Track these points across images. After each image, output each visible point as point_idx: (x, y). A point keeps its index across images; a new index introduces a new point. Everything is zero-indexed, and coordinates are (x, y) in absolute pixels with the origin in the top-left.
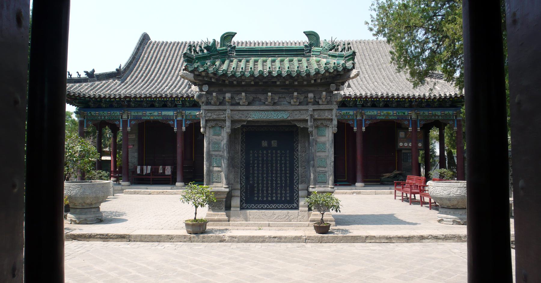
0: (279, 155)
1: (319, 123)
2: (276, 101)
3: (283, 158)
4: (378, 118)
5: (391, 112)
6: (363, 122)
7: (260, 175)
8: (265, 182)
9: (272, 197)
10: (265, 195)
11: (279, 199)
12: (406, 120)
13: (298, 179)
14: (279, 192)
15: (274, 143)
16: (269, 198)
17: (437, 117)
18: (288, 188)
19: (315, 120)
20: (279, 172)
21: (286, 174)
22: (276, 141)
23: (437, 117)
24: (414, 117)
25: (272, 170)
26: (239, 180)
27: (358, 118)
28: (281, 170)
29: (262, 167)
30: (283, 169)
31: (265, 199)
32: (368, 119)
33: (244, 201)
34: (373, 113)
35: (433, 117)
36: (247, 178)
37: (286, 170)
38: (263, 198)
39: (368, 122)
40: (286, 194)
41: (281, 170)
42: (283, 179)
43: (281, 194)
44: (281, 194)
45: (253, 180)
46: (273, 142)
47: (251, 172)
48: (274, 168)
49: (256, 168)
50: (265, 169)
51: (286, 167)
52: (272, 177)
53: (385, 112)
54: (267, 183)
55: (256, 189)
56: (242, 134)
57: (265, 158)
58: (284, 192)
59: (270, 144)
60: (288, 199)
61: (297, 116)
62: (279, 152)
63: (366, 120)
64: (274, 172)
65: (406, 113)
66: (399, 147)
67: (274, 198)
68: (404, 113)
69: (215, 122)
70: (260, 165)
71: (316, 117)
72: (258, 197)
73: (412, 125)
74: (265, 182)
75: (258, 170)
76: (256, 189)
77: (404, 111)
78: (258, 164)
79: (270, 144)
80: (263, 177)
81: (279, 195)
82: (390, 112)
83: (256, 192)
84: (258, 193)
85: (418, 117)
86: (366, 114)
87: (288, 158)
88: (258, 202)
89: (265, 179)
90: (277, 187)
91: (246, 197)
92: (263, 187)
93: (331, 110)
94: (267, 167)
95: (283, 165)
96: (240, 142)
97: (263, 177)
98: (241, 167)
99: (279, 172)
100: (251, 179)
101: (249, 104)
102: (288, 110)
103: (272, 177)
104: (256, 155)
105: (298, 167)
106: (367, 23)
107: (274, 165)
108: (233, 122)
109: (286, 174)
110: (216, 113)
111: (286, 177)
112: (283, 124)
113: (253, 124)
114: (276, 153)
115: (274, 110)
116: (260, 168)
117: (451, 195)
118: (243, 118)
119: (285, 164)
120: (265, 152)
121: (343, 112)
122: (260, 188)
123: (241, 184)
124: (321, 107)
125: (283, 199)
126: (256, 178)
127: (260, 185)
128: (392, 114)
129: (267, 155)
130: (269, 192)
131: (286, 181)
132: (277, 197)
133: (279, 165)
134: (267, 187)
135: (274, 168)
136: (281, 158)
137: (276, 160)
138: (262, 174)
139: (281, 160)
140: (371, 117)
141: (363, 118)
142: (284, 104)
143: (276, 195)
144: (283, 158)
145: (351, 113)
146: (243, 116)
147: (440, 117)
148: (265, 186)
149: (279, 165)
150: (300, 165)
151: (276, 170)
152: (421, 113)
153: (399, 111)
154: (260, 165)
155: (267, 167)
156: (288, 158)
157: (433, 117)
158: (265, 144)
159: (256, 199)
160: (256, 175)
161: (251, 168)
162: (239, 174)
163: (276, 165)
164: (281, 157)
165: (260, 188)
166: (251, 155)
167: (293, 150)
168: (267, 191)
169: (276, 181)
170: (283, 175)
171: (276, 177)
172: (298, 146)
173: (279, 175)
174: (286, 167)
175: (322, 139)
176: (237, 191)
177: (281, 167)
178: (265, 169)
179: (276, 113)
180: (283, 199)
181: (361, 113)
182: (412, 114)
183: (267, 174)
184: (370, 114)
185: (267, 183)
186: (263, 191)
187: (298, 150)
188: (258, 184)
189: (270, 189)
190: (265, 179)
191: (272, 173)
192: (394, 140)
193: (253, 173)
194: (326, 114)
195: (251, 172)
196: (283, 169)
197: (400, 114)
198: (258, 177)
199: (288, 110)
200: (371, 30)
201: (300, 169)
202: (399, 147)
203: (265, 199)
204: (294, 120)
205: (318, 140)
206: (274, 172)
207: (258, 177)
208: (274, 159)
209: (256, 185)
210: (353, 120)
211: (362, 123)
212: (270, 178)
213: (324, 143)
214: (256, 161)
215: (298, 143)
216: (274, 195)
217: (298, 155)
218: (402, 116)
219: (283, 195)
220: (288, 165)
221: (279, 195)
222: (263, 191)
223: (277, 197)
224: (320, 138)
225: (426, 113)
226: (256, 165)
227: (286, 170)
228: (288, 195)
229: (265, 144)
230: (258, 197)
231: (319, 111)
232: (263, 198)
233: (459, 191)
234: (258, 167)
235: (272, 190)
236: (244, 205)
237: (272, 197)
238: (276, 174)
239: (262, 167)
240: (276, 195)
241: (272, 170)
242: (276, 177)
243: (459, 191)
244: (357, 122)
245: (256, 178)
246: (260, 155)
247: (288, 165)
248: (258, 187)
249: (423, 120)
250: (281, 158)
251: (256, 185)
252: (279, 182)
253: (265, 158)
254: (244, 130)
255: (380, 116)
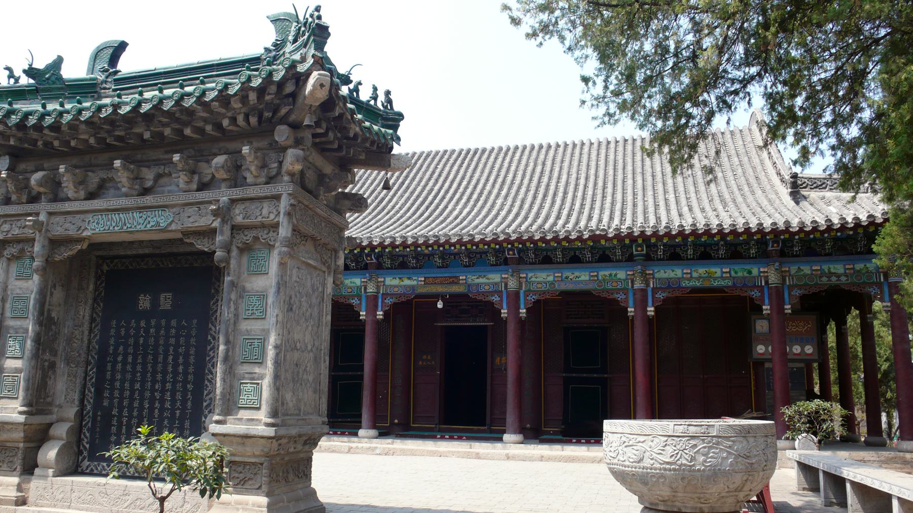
1: (248, 237)
2: (149, 184)
3: (182, 340)
4: (685, 284)
5: (717, 271)
6: (650, 294)
8: (136, 404)
12: (755, 286)
15: (166, 301)
17: (834, 279)
19: (236, 229)
20: (169, 377)
23: (834, 279)
24: (773, 278)
25: (154, 373)
27: (638, 285)
28: (175, 373)
30: (181, 369)
32: (660, 288)
33: (85, 454)
34: (672, 275)
35: (825, 279)
37: (186, 373)
39: (660, 296)
41: (175, 373)
42: (179, 396)
45: (111, 398)
48: (160, 367)
51: (186, 364)
53: (702, 271)
56: (98, 278)
57: (141, 341)
59: (155, 303)
61: (191, 220)
62: (174, 323)
63: (655, 290)
65: (755, 272)
66: (755, 356)
68: (750, 272)
69: (20, 246)
70: (130, 359)
71: (239, 219)
73: (769, 298)
74: (136, 404)
77: (748, 267)
78: (125, 355)
79: (155, 303)
82: (713, 270)
83: (114, 429)
85: (784, 280)
86: (657, 275)
87: (193, 341)
93: (277, 198)
95: (181, 360)
99: (169, 377)
100: (106, 394)
101: (91, 196)
102: (173, 206)
103: (153, 390)
104: (123, 333)
106: (506, 8)
107: (161, 358)
108: (55, 243)
109: (185, 382)
110: (19, 224)
111: (185, 391)
113: (122, 253)
114: (168, 327)
115: (141, 209)
117: (647, 463)
118: (72, 232)
119: (186, 355)
121: (601, 273)
124: (252, 192)
126: (116, 394)
128: (718, 274)
129: (147, 331)
131: (184, 401)
133: (171, 358)
139: (177, 346)
140: (669, 285)
141: (648, 285)
142: (169, 192)
145: (622, 274)
146: (73, 227)
147: (843, 279)
151: (165, 373)
152: (794, 269)
153: (736, 268)
154: (130, 359)
155: (144, 364)
157: (825, 279)
158: (144, 302)
160: (118, 384)
161: (109, 367)
164: (177, 337)
166: (113, 332)
169: (162, 401)
171: (163, 391)
173: (169, 386)
174: (186, 364)
175: (258, 283)
177: (176, 365)
181: (643, 274)
182: (767, 273)
183: (143, 382)
184: (666, 276)
191: (154, 381)
192: (743, 338)
193: (113, 380)
194: (265, 212)
197: (740, 274)
198: (122, 390)
199: (173, 206)
200: (516, 22)
202: (755, 356)
204: (187, 233)
205: (248, 286)
207: (122, 390)
208: (161, 342)
210: (625, 291)
211: (647, 296)
212: (148, 394)
213: (262, 296)
214: (121, 348)
218: (744, 278)
220: (192, 360)
224: (254, 278)
225: (806, 270)
227: (186, 373)
229: (144, 302)
231: (247, 204)
233: (670, 449)
234: (125, 363)
238: (164, 382)
241: (154, 373)
243: (670, 449)
244: (634, 294)
245: (116, 394)
246: (132, 332)
247: (192, 360)
248: (120, 416)
249: (800, 287)
250: (177, 341)
251: (115, 412)
253: (141, 341)
254: (105, 268)
255: (690, 279)
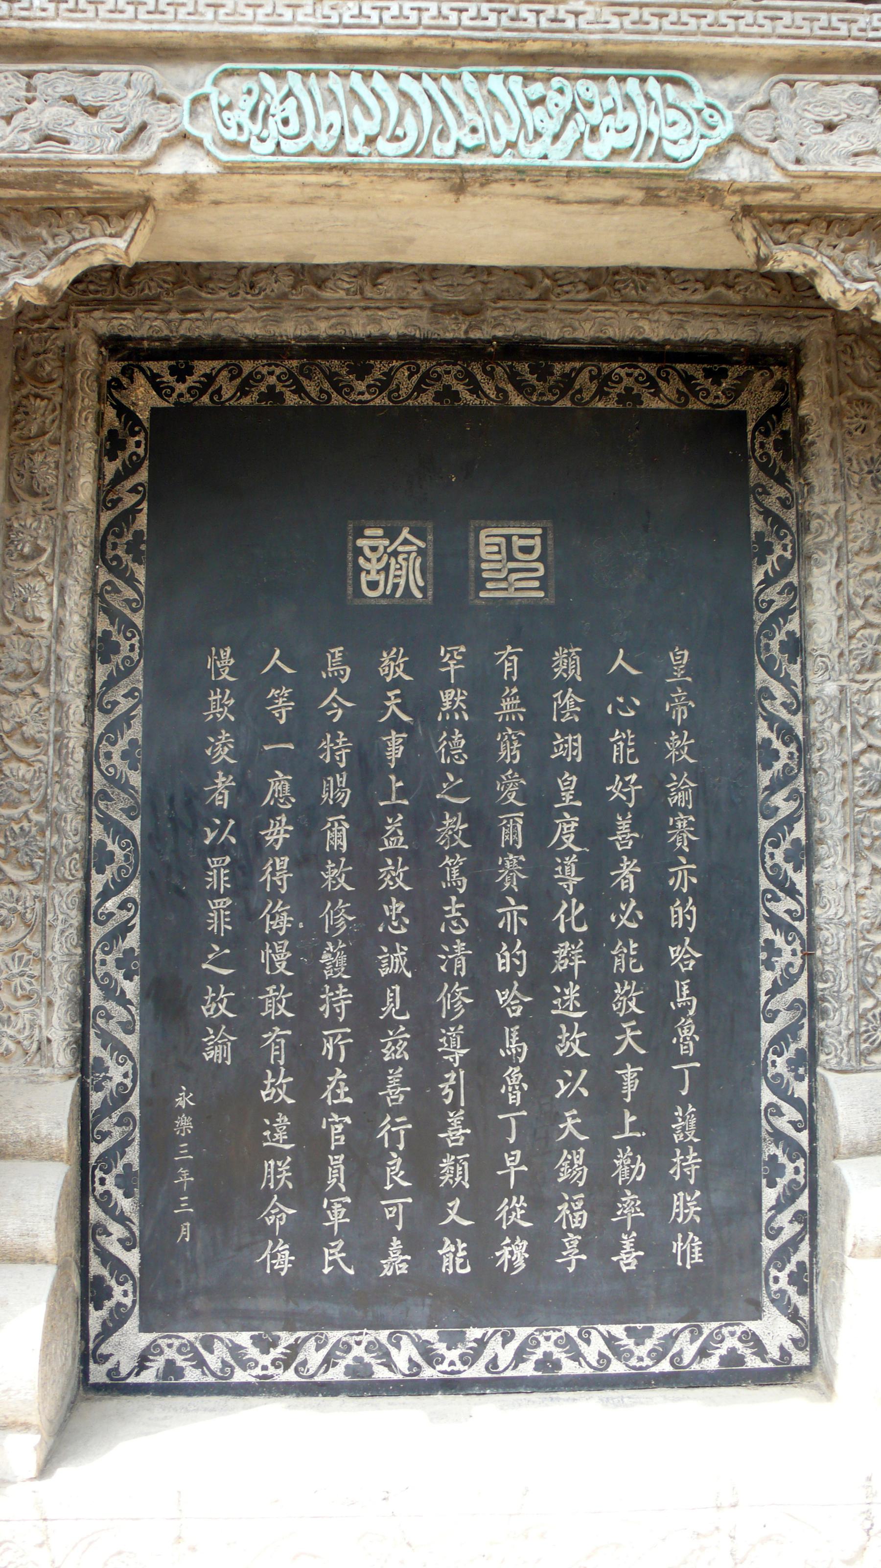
0: (569, 703)
3: (621, 745)
7: (333, 960)
8: (395, 1048)
9: (483, 1240)
10: (395, 1209)
11: (572, 1255)
13: (813, 1007)
14: (573, 1167)
15: (511, 560)
16: (453, 1256)
18: (685, 1124)
20: (569, 914)
21: (657, 933)
22: (529, 535)
25: (483, 895)
26: (58, 1028)
28: (598, 894)
29: (364, 859)
30: (627, 874)
31: (396, 1262)
33: (122, 1294)
36: (169, 1001)
37: (655, 896)
38: (366, 1242)
40: (658, 1188)
41: (598, 894)
43: (602, 1191)
44: (602, 1191)
45: (248, 1025)
46: (489, 541)
47: (219, 914)
48: (511, 871)
49: (278, 871)
50: (394, 876)
51: (654, 853)
52: (482, 981)
54: (425, 1066)
55: (279, 1134)
56: (112, 444)
57: (395, 746)
58: (628, 1167)
59: (452, 570)
60: (689, 1250)
62: (566, 662)
64: (512, 915)
67: (514, 1254)
70: (338, 835)
72: (308, 1239)
75: (308, 893)
76: (279, 1134)
78: (309, 817)
79: (452, 570)
80: (367, 988)
81: (574, 1214)
83: (278, 1172)
84: (309, 1188)
88: (310, 1302)
89: (392, 1003)
90: (543, 1112)
91: (156, 1242)
92: (367, 1109)
94: (422, 858)
95: (624, 834)
96: (82, 530)
97: (367, 988)
98: (94, 858)
99: (569, 914)
100: (216, 1005)
103: (482, 981)
104: (281, 706)
105: (805, 855)
107: (513, 830)
109: (657, 933)
111: (658, 979)
112: (620, 325)
114: (538, 686)
116: (334, 875)
119: (652, 814)
120: (392, 665)
122: (337, 1128)
123: (85, 1070)
125: (628, 1259)
126: (275, 1002)
127: (337, 1089)
129: (421, 701)
130: (453, 1171)
131: (658, 1019)
132: (544, 1242)
133: (567, 829)
134: (426, 1114)
135: (511, 871)
136: (598, 749)
137: (540, 768)
138: (363, 945)
139: (596, 771)
143: (542, 1203)
144: (621, 745)
146: (83, 124)
148: (395, 1092)
149: (567, 829)
150: (833, 821)
151: (540, 895)
154: (338, 835)
155: (422, 858)
156: (678, 746)
158: (390, 563)
159: (281, 1258)
160: (278, 957)
162: (62, 949)
163: (540, 824)
164: (594, 727)
165: (337, 1128)
166: (220, 706)
167: (736, 643)
168: (423, 1154)
169: (540, 1028)
170: (624, 955)
171: (541, 982)
172: (799, 593)
173: (568, 956)
174: (654, 853)
176: (29, 1167)
177: (598, 860)
178: (394, 876)
179: (560, 92)
180: (628, 1259)
183: (425, 945)
185: (425, 1066)
186: (365, 1158)
187: (796, 647)
188: (308, 1070)
189: (456, 1133)
190: (392, 1003)
191: (486, 937)
193: (247, 936)
195: (219, 914)
196: (627, 874)
198: (306, 986)
199: (719, 66)
201: (833, 872)
203: (396, 1262)
206: (512, 915)
207: (306, 986)
208: (510, 750)
209: (275, 1088)
212: (455, 999)
214: (280, 785)
215: (801, 557)
216: (513, 1210)
217: (802, 705)
219: (630, 1207)
220: (682, 832)
221: (574, 1214)
222: (365, 1158)
223: (544, 1242)
226: (277, 833)
227: (655, 896)
228: (686, 1206)
230: (308, 1239)
232: (366, 1242)
234: (307, 854)
235: (484, 1151)
236: (131, 1340)
237: (483, 1240)
238: (541, 940)
239: (364, 859)
240: (542, 1203)
241: (483, 895)
242: (541, 982)
245: (275, 1002)
246: (335, 704)
247: (682, 832)
251: (275, 1088)
252: (570, 1044)
253: (395, 746)
254: (142, 398)
